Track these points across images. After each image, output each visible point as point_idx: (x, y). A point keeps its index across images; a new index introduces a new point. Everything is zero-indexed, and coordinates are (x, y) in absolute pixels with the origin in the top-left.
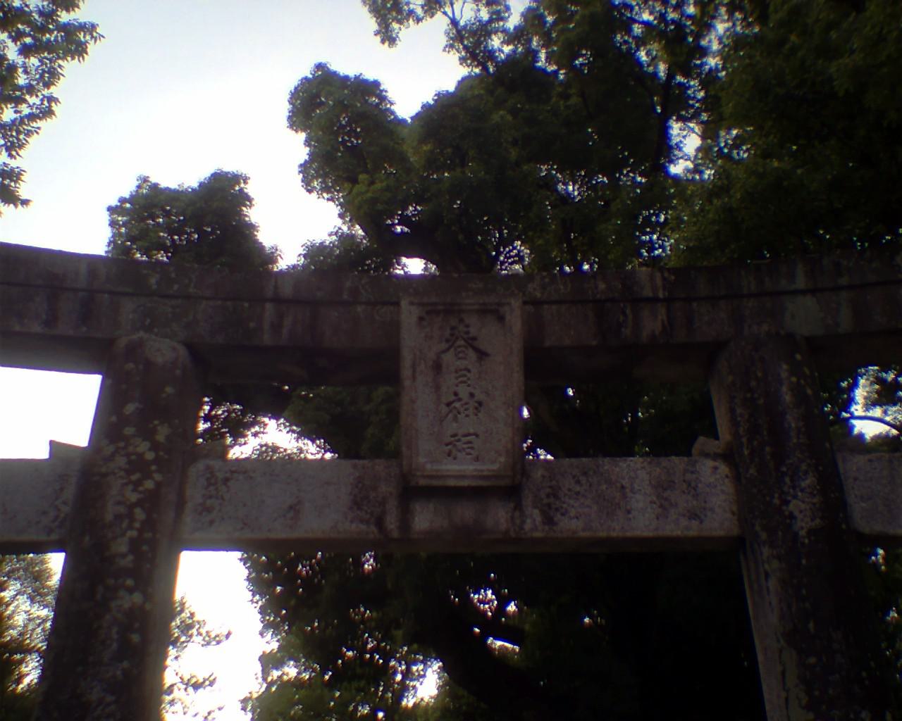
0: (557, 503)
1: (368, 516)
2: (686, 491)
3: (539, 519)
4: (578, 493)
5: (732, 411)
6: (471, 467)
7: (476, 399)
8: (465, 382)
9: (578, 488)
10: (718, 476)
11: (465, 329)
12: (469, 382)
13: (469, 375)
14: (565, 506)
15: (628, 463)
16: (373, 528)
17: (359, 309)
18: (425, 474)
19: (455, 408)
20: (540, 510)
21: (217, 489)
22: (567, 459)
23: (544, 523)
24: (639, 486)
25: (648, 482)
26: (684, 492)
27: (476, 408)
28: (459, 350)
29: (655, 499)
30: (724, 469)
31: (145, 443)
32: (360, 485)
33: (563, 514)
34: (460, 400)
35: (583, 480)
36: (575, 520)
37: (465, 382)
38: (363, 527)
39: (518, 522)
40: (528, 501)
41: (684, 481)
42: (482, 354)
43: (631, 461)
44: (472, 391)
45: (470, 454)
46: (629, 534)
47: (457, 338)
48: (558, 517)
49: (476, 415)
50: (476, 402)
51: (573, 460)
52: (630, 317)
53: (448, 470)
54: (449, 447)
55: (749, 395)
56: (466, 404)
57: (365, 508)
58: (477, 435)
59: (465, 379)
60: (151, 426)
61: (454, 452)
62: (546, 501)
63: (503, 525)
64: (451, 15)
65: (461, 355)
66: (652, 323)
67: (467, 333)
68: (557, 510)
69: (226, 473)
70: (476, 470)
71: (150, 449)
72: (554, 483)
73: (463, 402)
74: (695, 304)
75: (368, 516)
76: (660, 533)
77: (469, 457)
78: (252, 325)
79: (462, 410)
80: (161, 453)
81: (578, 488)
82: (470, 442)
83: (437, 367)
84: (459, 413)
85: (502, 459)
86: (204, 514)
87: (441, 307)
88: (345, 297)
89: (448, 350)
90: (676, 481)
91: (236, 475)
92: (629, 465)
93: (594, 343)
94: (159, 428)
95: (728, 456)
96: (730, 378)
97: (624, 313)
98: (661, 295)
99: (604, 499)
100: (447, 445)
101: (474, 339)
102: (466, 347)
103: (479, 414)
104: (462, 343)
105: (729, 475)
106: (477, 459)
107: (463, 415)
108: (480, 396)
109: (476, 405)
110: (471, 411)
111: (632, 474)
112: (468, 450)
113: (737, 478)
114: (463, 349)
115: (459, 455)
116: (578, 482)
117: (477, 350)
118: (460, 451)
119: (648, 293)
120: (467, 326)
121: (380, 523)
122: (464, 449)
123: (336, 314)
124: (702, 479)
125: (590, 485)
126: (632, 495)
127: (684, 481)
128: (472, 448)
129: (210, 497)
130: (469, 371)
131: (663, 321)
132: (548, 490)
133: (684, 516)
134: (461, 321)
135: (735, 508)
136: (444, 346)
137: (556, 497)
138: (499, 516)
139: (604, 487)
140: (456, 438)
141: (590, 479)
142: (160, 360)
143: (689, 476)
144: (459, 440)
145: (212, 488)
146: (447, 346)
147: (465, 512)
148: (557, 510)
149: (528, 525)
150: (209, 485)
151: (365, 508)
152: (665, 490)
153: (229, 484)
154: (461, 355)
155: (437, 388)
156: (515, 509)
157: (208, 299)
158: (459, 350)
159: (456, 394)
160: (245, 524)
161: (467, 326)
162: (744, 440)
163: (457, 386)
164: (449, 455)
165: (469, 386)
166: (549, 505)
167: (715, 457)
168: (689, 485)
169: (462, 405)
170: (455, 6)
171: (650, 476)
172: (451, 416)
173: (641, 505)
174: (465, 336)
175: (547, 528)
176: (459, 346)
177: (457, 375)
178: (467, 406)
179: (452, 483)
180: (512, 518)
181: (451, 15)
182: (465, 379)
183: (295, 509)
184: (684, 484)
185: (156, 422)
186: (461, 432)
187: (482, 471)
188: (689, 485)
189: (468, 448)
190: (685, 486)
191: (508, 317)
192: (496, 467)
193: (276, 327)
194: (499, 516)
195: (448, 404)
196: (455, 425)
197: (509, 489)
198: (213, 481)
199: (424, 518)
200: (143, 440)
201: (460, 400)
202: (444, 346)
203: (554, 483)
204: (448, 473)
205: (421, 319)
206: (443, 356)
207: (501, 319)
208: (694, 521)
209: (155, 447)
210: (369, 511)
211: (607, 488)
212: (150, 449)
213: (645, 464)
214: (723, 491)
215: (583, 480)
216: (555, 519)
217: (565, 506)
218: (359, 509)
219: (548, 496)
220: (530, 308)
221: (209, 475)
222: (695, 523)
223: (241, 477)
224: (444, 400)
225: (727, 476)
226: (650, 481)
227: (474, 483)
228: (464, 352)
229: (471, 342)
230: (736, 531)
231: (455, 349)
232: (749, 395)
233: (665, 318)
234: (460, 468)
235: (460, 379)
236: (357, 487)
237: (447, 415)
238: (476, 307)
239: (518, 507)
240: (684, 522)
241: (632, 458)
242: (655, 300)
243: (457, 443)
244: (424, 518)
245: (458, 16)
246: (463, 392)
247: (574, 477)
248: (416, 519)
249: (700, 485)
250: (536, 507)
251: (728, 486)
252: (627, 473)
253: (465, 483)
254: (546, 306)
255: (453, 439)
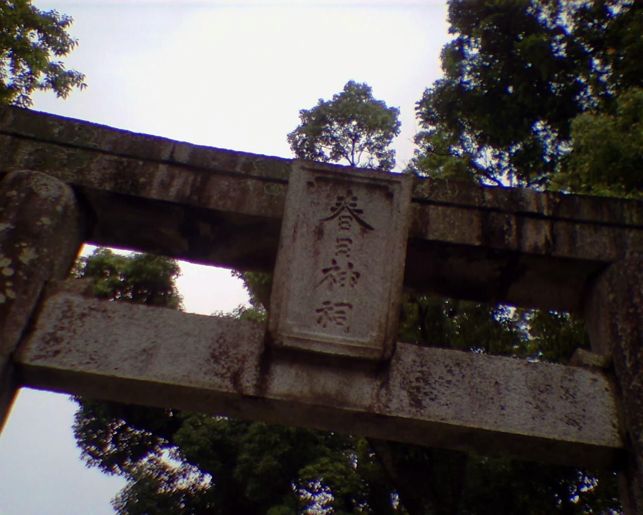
0: (427, 387)
1: (224, 371)
2: (564, 397)
3: (406, 401)
4: (449, 382)
5: (613, 326)
6: (340, 337)
7: (354, 270)
8: (345, 252)
9: (450, 378)
10: (597, 388)
11: (352, 202)
12: (349, 253)
13: (350, 246)
14: (435, 392)
15: (504, 362)
16: (227, 383)
17: (250, 182)
18: (291, 336)
19: (331, 275)
20: (408, 392)
21: (70, 322)
22: (440, 349)
23: (411, 405)
24: (515, 385)
25: (524, 383)
26: (561, 397)
27: (353, 279)
28: (344, 220)
29: (531, 399)
30: (603, 382)
31: (6, 260)
32: (221, 341)
33: (432, 399)
34: (337, 268)
35: (456, 370)
36: (446, 407)
37: (345, 252)
38: (217, 380)
39: (384, 400)
40: (396, 380)
41: (562, 387)
42: (366, 227)
43: (507, 360)
44: (352, 262)
45: (339, 324)
46: (502, 430)
47: (343, 209)
48: (426, 401)
49: (352, 286)
50: (354, 273)
51: (446, 351)
52: (514, 227)
53: (316, 336)
54: (321, 314)
55: (631, 311)
56: (344, 273)
57: (223, 363)
58: (350, 306)
59: (344, 249)
60: (17, 246)
61: (324, 320)
62: (414, 384)
63: (367, 402)
64: (351, 160)
65: (344, 225)
66: (535, 236)
67: (355, 205)
68: (426, 394)
69: (85, 309)
70: (344, 340)
71: (10, 266)
72: (425, 369)
73: (341, 271)
74: (578, 227)
75: (224, 371)
76: (537, 434)
77: (340, 327)
78: (142, 180)
79: (338, 279)
80: (21, 273)
81: (450, 378)
82: (343, 312)
83: (319, 233)
84: (335, 281)
85: (374, 334)
86: (52, 343)
87: (330, 176)
88: (238, 169)
89: (332, 218)
90: (554, 386)
91: (94, 312)
92: (504, 364)
93: (477, 244)
94: (25, 250)
95: (608, 370)
96: (611, 297)
97: (509, 224)
98: (545, 213)
99: (477, 392)
100: (318, 311)
101: (360, 212)
102: (351, 219)
103: (355, 286)
104: (348, 214)
105: (608, 387)
106: (348, 330)
107: (339, 284)
108: (357, 267)
109: (354, 276)
110: (347, 282)
111: (508, 373)
112: (340, 320)
113: (617, 391)
114: (348, 220)
115: (329, 323)
116: (450, 371)
117: (361, 222)
118: (330, 319)
119: (532, 208)
120: (355, 199)
121: (236, 378)
122: (335, 318)
123: (227, 183)
124: (581, 388)
125: (463, 376)
126: (507, 393)
127: (562, 387)
128: (344, 318)
129: (62, 329)
130: (350, 241)
131: (546, 236)
132: (418, 374)
133: (561, 420)
134: (349, 193)
135: (615, 421)
136: (330, 214)
137: (426, 382)
138: (362, 393)
139: (478, 380)
140: (329, 306)
141: (463, 371)
142: (43, 193)
143: (566, 384)
144: (331, 309)
145: (66, 321)
146: (332, 214)
147: (328, 383)
148: (426, 394)
149: (394, 405)
150: (65, 317)
151: (223, 363)
152: (542, 392)
153: (84, 319)
154: (344, 225)
155: (317, 253)
156: (382, 386)
157: (104, 152)
158: (344, 220)
159: (334, 262)
160: (93, 359)
161: (355, 199)
162: (627, 353)
163: (336, 254)
164: (319, 322)
165: (348, 256)
166: (418, 389)
167: (594, 369)
168: (567, 391)
169: (339, 275)
170: (355, 155)
171: (527, 377)
172: (326, 283)
173: (516, 403)
174: (351, 208)
175: (414, 410)
176: (344, 217)
177: (338, 244)
178: (344, 276)
179: (317, 349)
180: (378, 395)
181: (351, 160)
182: (344, 249)
183: (148, 353)
184: (562, 389)
185: (24, 244)
186: (334, 301)
187: (352, 342)
188: (567, 391)
189: (340, 318)
190: (563, 392)
191: (396, 196)
192: (366, 340)
193: (165, 186)
194: (362, 393)
195: (325, 271)
196: (328, 293)
197: (378, 367)
198: (69, 314)
199: (285, 382)
200: (5, 257)
201: (337, 268)
202: (330, 214)
203: (425, 369)
204: (315, 339)
205: (310, 184)
206: (326, 223)
207: (390, 196)
208: (572, 427)
209: (16, 265)
210: (226, 366)
211: (480, 382)
212: (10, 266)
213: (521, 366)
214: (603, 403)
215: (456, 370)
216: (424, 403)
217: (435, 392)
218: (216, 362)
219: (417, 379)
220: (418, 206)
221: (65, 308)
222: (573, 429)
223: (99, 315)
224: (322, 267)
225: (607, 390)
226: (526, 381)
227: (341, 352)
228: (347, 222)
229: (356, 214)
230: (617, 444)
231: (340, 219)
232: (631, 311)
233: (548, 234)
234: (330, 337)
235: (340, 249)
236: (217, 342)
237: (322, 281)
238: (366, 181)
239: (385, 384)
240: (562, 426)
241: (507, 358)
242: (538, 216)
243: (329, 312)
244: (285, 382)
245: (356, 160)
246: (342, 262)
247: (446, 366)
248: (275, 381)
249: (578, 394)
250: (404, 389)
251: (609, 400)
252: (503, 371)
253: (332, 351)
254: (432, 207)
255: (324, 306)
